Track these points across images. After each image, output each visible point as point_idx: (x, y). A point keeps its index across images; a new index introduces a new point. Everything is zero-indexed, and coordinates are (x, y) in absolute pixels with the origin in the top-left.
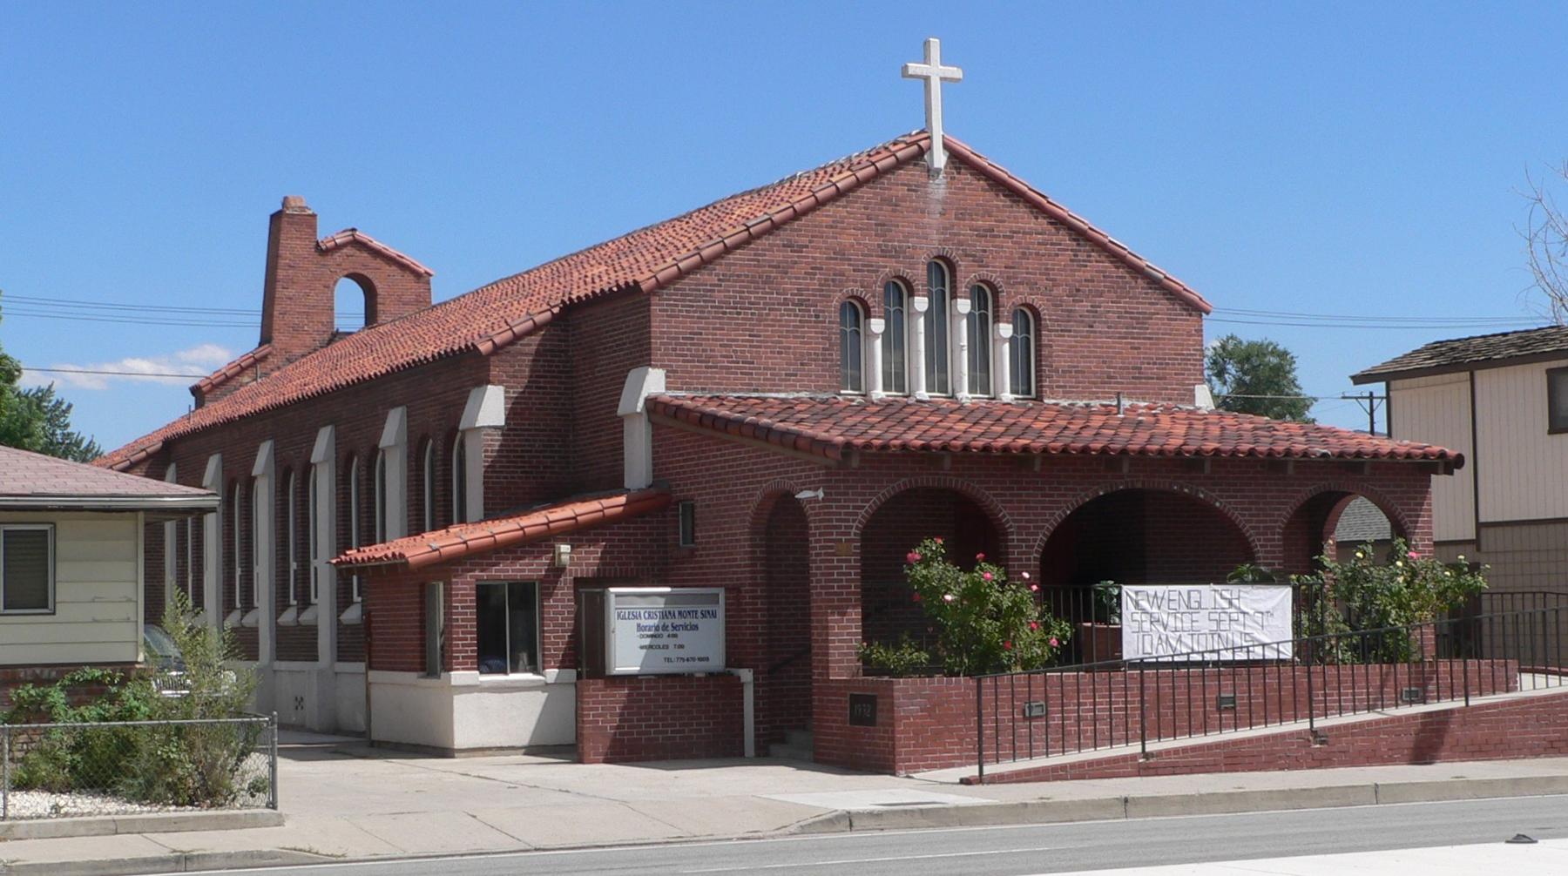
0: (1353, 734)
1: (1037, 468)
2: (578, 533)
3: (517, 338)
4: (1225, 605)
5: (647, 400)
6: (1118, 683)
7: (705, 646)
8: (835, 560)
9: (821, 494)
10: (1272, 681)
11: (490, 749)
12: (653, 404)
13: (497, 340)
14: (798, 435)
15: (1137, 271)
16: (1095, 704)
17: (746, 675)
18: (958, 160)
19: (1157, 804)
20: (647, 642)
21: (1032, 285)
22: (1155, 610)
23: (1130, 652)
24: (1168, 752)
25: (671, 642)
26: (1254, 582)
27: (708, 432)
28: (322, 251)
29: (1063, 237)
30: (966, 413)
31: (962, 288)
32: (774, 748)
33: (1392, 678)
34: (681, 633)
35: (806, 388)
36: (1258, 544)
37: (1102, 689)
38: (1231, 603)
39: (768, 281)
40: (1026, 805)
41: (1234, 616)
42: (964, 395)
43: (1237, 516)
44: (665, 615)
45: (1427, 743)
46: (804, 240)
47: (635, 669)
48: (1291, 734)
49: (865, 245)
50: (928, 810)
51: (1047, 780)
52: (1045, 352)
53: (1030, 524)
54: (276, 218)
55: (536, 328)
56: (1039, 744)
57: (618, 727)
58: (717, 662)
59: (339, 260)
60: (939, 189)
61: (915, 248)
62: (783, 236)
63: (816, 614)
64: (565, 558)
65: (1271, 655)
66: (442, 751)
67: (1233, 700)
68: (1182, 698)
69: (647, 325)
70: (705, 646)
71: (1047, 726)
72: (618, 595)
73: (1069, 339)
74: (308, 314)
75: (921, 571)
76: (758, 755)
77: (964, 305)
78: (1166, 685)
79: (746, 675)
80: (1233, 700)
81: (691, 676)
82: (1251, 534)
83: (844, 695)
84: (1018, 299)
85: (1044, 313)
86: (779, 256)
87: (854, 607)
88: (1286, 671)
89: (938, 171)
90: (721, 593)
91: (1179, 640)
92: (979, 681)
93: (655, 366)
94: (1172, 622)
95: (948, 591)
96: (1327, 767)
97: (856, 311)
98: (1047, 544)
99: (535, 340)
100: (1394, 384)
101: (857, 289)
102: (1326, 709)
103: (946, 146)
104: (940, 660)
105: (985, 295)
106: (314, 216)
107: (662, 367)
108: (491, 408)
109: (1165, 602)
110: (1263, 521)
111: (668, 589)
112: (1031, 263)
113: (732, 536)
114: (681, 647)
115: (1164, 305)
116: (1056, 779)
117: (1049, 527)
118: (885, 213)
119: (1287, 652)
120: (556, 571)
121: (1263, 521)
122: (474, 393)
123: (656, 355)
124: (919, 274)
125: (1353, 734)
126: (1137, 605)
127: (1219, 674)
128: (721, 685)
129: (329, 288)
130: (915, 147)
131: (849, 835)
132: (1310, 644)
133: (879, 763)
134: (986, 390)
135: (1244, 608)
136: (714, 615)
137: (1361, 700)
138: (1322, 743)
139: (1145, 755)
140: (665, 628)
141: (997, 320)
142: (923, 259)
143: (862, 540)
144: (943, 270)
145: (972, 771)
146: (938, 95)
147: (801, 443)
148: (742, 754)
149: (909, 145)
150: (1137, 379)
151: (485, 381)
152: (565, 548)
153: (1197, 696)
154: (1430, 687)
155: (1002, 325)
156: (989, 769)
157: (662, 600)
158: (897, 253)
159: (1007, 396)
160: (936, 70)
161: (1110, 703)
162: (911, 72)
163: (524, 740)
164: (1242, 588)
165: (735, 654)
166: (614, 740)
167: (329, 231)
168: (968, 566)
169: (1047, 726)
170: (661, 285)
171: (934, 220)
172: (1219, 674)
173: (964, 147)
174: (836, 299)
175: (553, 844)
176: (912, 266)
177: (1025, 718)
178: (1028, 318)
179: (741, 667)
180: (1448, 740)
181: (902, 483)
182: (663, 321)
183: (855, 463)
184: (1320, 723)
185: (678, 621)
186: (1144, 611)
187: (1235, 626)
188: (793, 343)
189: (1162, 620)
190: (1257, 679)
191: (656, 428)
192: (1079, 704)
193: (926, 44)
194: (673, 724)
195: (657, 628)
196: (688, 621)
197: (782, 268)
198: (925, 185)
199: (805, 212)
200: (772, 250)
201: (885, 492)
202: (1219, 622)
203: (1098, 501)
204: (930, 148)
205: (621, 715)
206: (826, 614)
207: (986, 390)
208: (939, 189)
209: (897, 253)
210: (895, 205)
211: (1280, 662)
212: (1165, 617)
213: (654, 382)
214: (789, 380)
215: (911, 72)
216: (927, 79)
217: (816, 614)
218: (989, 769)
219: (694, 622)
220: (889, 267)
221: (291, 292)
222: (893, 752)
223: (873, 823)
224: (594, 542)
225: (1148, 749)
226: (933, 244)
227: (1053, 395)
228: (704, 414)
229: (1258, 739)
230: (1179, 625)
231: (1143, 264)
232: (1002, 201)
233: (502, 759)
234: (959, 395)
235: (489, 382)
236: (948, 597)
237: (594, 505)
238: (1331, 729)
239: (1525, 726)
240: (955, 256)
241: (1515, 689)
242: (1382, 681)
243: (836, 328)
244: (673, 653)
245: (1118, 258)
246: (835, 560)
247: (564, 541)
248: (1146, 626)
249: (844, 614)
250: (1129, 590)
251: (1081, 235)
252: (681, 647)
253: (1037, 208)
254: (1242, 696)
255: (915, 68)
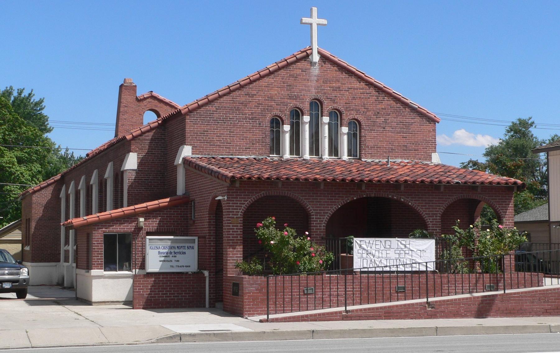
0: (447, 304)
1: (322, 187)
2: (148, 214)
3: (143, 133)
4: (403, 247)
5: (183, 158)
6: (349, 280)
7: (188, 261)
8: (233, 225)
9: (226, 198)
10: (423, 280)
11: (108, 302)
12: (185, 160)
13: (134, 134)
14: (219, 173)
15: (406, 105)
16: (456, 287)
17: (206, 273)
18: (324, 58)
19: (328, 333)
20: (163, 259)
21: (357, 111)
22: (369, 249)
23: (358, 264)
24: (357, 310)
25: (173, 259)
26: (419, 237)
27: (198, 172)
28: (139, 100)
29: (372, 90)
30: (325, 166)
31: (326, 112)
32: (218, 305)
33: (481, 280)
34: (178, 255)
35: (254, 154)
36: (429, 221)
37: (342, 282)
38: (405, 246)
39: (238, 109)
40: (265, 332)
41: (407, 252)
42: (307, 156)
43: (420, 209)
44: (171, 248)
45: (484, 309)
46: (255, 92)
47: (157, 270)
48: (417, 304)
49: (282, 94)
50: (218, 334)
51: (299, 321)
52: (363, 139)
53: (321, 213)
54: (121, 86)
55: (151, 129)
56: (311, 306)
57: (149, 294)
58: (193, 267)
59: (145, 104)
60: (316, 70)
61: (304, 95)
62: (245, 90)
63: (225, 248)
64: (142, 224)
65: (423, 268)
66: (87, 302)
67: (404, 288)
68: (379, 287)
69: (184, 128)
70: (188, 261)
71: (315, 298)
72: (150, 239)
73: (374, 134)
74: (132, 125)
75: (261, 231)
76: (210, 307)
77: (326, 119)
78: (372, 281)
79: (206, 273)
80: (404, 288)
81: (187, 273)
82: (426, 217)
83: (231, 283)
84: (351, 117)
85: (363, 123)
86: (243, 99)
87: (240, 245)
88: (431, 276)
89: (315, 63)
90: (196, 238)
91: (381, 261)
92: (268, 278)
93: (188, 145)
94: (377, 254)
95: (272, 239)
96: (434, 318)
97: (276, 123)
98: (329, 220)
99: (151, 134)
100: (551, 153)
101: (278, 113)
102: (449, 293)
103: (319, 53)
104: (270, 268)
105: (336, 115)
106: (136, 86)
107: (190, 145)
108: (132, 162)
109: (374, 246)
110: (431, 213)
111: (172, 237)
112: (357, 102)
113: (202, 217)
114: (178, 261)
115: (418, 119)
116: (303, 321)
117: (330, 213)
118: (291, 81)
119: (431, 267)
120: (139, 229)
121: (431, 213)
122: (127, 155)
123: (188, 140)
124: (306, 106)
125: (447, 304)
126: (360, 246)
127: (405, 277)
128: (198, 275)
129: (141, 115)
130: (305, 53)
131: (180, 343)
132: (443, 265)
133: (234, 311)
134: (317, 154)
135: (412, 248)
136: (193, 248)
137: (466, 289)
138: (432, 308)
139: (347, 311)
140: (171, 253)
141: (341, 126)
142: (308, 100)
143: (243, 217)
144: (317, 105)
145: (265, 317)
146: (316, 32)
147: (220, 176)
148: (204, 306)
149: (302, 52)
150: (405, 151)
151: (130, 151)
152: (142, 220)
153: (387, 286)
154: (500, 284)
155: (343, 128)
156: (271, 316)
157: (170, 242)
158: (296, 98)
159: (345, 157)
160: (315, 20)
161: (338, 288)
162: (303, 21)
163: (123, 299)
164: (414, 240)
165: (201, 265)
166: (147, 300)
167: (141, 92)
168: (281, 230)
169: (315, 298)
170: (190, 111)
171: (314, 84)
172: (405, 277)
173: (327, 53)
174: (269, 117)
175: (39, 345)
176: (303, 103)
177: (305, 294)
178: (355, 125)
179: (205, 270)
180: (494, 307)
181: (263, 193)
182: (191, 126)
183: (237, 185)
184: (430, 300)
185: (177, 250)
186: (364, 249)
187: (407, 256)
188: (249, 135)
189: (371, 253)
190: (416, 281)
191: (186, 170)
192: (330, 289)
193: (311, 9)
194: (165, 294)
195: (167, 253)
196: (181, 250)
197: (244, 104)
198: (309, 69)
199: (255, 81)
200: (240, 97)
201: (253, 198)
202: (400, 254)
203: (353, 202)
204: (312, 53)
205: (151, 289)
206: (227, 248)
207: (317, 154)
208: (316, 70)
209: (296, 98)
210: (295, 77)
211: (426, 272)
212: (374, 252)
213: (186, 152)
214: (246, 150)
215: (303, 21)
216: (311, 24)
217: (225, 248)
218: (271, 316)
219: (184, 251)
220: (292, 104)
221: (126, 116)
222: (243, 308)
223: (191, 339)
224: (156, 217)
225: (344, 308)
226: (313, 93)
227: (366, 157)
228: (196, 165)
229: (401, 305)
230: (380, 255)
231: (408, 102)
232: (344, 75)
233: (113, 306)
234: (323, 157)
235: (131, 151)
236: (272, 242)
237: (156, 202)
238: (436, 302)
239: (533, 302)
240: (322, 98)
241: (543, 286)
242: (476, 281)
243: (268, 129)
244: (174, 264)
245: (397, 100)
246: (233, 225)
247: (142, 217)
248: (365, 255)
249: (235, 248)
250: (355, 239)
251: (380, 90)
252: (178, 261)
253: (360, 78)
254: (408, 287)
255: (305, 20)
